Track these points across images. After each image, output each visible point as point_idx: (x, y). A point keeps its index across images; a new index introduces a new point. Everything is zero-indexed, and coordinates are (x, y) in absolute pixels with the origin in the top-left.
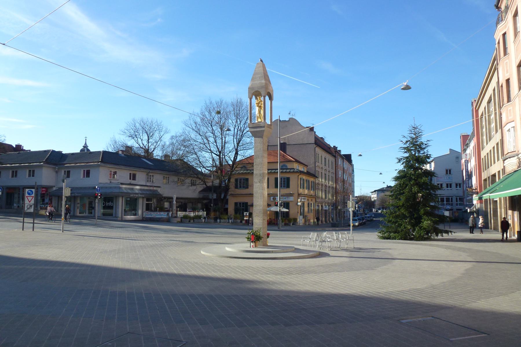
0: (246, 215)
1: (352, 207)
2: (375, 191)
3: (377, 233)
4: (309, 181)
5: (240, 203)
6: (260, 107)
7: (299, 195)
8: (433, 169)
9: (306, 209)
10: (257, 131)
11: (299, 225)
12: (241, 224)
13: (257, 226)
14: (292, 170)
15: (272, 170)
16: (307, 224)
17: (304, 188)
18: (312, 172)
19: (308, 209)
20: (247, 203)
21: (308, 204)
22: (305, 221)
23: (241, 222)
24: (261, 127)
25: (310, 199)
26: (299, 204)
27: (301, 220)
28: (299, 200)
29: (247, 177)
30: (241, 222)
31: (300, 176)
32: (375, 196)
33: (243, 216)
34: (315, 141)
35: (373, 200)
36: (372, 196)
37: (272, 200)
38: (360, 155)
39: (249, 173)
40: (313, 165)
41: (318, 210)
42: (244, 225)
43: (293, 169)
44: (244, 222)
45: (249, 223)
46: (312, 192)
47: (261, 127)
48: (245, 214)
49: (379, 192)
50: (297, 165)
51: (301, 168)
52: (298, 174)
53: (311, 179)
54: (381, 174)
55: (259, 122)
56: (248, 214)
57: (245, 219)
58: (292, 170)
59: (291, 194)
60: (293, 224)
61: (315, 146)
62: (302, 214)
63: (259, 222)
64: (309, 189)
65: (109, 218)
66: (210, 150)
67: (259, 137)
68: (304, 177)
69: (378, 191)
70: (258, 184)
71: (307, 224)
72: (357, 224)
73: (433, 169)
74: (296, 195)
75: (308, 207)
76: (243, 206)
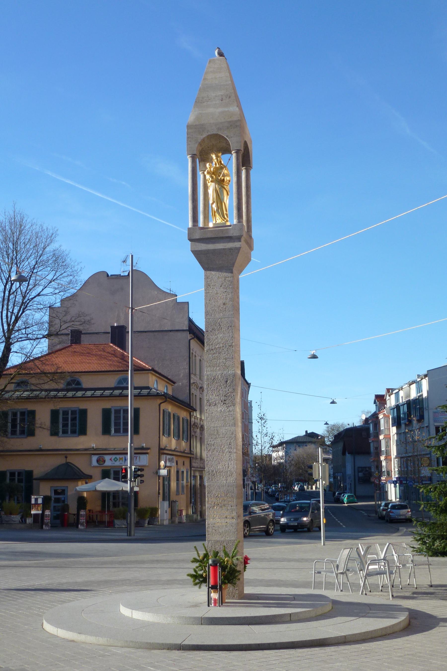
0: (36, 503)
1: (323, 478)
2: (281, 444)
3: (410, 539)
4: (178, 418)
5: (12, 474)
6: (221, 182)
7: (162, 451)
8: (425, 395)
9: (173, 485)
10: (214, 252)
11: (162, 525)
12: (23, 526)
13: (217, 538)
14: (145, 392)
15: (104, 389)
16: (177, 520)
17: (169, 435)
18: (183, 397)
19: (178, 484)
20: (29, 474)
21: (178, 472)
22: (172, 515)
23: (23, 520)
24: (230, 239)
25: (180, 461)
26: (163, 472)
27: (163, 512)
28: (162, 463)
29: (30, 407)
30: (23, 520)
31: (163, 406)
32: (281, 453)
33: (29, 507)
34: (190, 327)
35: (274, 463)
36: (274, 455)
37: (94, 463)
38: (314, 357)
39: (36, 397)
40: (186, 382)
41: (195, 486)
42: (30, 528)
43: (148, 388)
44: (29, 521)
45: (43, 523)
46: (184, 444)
47: (230, 239)
48: (33, 501)
49: (292, 447)
50: (154, 378)
51: (161, 387)
52: (159, 401)
53: (183, 414)
54: (333, 402)
55: (217, 226)
56: (40, 501)
57: (33, 512)
58: (145, 392)
59: (143, 448)
60: (149, 524)
61: (189, 336)
62: (166, 496)
63: (222, 521)
64: (179, 437)
65: (159, 556)
66: (39, 309)
67: (220, 269)
68: (170, 408)
69: (287, 443)
70: (221, 408)
71: (177, 520)
72: (283, 520)
73: (425, 395)
74: (155, 451)
75: (178, 480)
76: (20, 481)
